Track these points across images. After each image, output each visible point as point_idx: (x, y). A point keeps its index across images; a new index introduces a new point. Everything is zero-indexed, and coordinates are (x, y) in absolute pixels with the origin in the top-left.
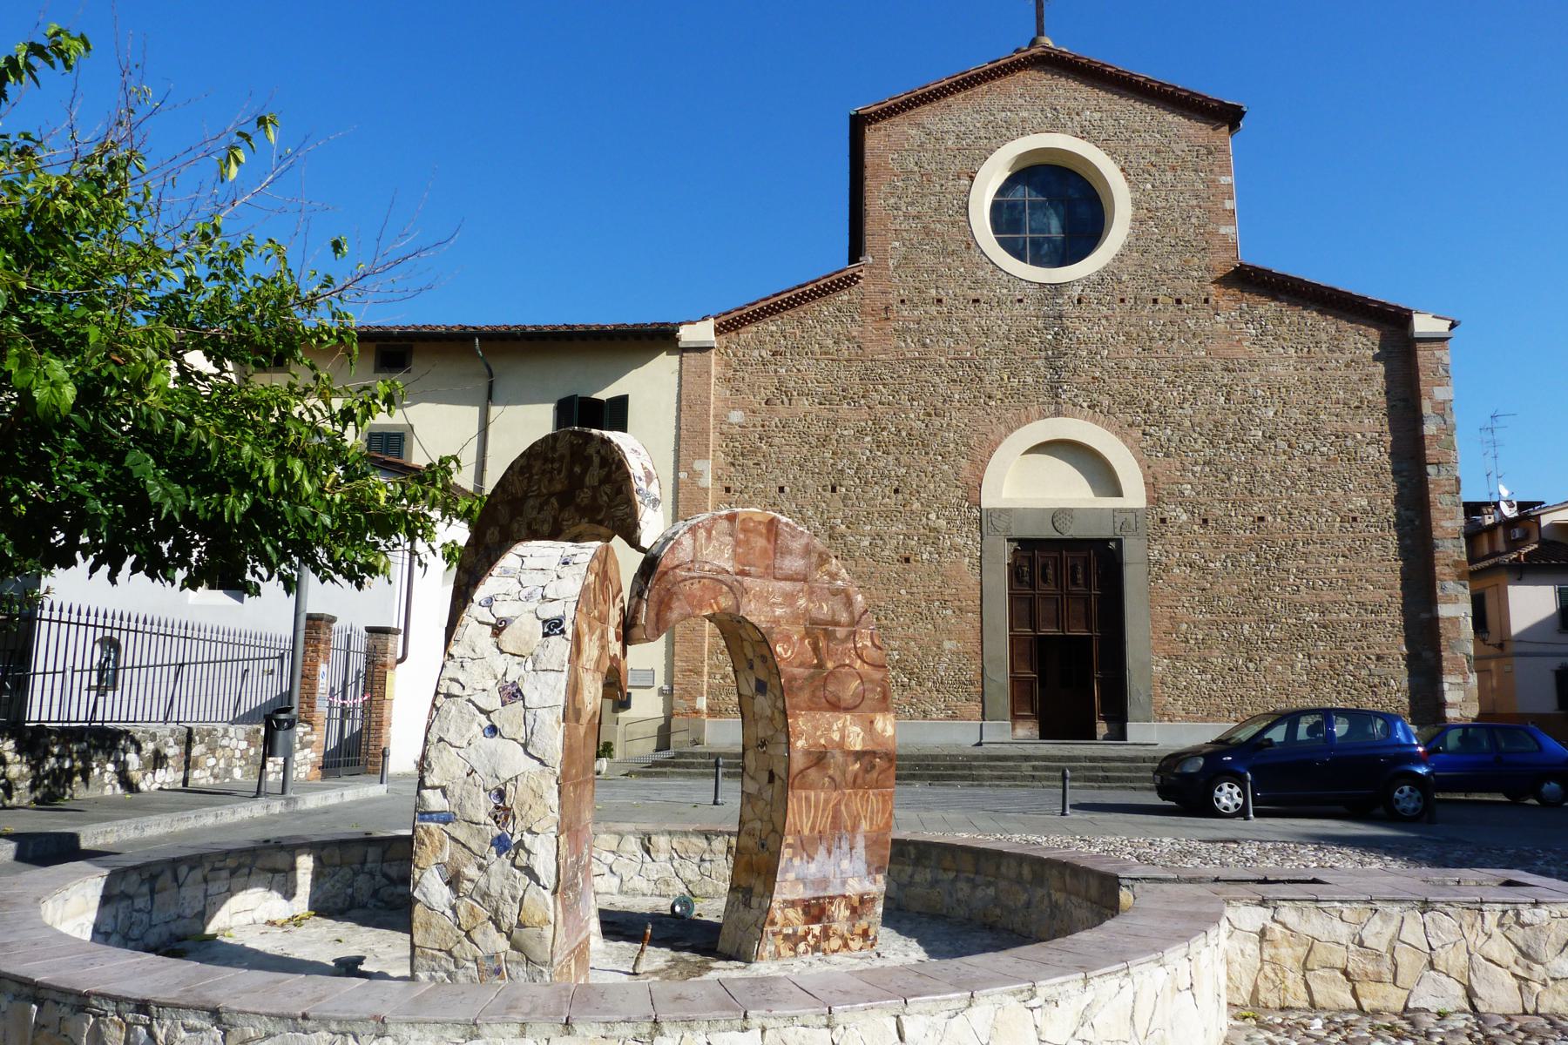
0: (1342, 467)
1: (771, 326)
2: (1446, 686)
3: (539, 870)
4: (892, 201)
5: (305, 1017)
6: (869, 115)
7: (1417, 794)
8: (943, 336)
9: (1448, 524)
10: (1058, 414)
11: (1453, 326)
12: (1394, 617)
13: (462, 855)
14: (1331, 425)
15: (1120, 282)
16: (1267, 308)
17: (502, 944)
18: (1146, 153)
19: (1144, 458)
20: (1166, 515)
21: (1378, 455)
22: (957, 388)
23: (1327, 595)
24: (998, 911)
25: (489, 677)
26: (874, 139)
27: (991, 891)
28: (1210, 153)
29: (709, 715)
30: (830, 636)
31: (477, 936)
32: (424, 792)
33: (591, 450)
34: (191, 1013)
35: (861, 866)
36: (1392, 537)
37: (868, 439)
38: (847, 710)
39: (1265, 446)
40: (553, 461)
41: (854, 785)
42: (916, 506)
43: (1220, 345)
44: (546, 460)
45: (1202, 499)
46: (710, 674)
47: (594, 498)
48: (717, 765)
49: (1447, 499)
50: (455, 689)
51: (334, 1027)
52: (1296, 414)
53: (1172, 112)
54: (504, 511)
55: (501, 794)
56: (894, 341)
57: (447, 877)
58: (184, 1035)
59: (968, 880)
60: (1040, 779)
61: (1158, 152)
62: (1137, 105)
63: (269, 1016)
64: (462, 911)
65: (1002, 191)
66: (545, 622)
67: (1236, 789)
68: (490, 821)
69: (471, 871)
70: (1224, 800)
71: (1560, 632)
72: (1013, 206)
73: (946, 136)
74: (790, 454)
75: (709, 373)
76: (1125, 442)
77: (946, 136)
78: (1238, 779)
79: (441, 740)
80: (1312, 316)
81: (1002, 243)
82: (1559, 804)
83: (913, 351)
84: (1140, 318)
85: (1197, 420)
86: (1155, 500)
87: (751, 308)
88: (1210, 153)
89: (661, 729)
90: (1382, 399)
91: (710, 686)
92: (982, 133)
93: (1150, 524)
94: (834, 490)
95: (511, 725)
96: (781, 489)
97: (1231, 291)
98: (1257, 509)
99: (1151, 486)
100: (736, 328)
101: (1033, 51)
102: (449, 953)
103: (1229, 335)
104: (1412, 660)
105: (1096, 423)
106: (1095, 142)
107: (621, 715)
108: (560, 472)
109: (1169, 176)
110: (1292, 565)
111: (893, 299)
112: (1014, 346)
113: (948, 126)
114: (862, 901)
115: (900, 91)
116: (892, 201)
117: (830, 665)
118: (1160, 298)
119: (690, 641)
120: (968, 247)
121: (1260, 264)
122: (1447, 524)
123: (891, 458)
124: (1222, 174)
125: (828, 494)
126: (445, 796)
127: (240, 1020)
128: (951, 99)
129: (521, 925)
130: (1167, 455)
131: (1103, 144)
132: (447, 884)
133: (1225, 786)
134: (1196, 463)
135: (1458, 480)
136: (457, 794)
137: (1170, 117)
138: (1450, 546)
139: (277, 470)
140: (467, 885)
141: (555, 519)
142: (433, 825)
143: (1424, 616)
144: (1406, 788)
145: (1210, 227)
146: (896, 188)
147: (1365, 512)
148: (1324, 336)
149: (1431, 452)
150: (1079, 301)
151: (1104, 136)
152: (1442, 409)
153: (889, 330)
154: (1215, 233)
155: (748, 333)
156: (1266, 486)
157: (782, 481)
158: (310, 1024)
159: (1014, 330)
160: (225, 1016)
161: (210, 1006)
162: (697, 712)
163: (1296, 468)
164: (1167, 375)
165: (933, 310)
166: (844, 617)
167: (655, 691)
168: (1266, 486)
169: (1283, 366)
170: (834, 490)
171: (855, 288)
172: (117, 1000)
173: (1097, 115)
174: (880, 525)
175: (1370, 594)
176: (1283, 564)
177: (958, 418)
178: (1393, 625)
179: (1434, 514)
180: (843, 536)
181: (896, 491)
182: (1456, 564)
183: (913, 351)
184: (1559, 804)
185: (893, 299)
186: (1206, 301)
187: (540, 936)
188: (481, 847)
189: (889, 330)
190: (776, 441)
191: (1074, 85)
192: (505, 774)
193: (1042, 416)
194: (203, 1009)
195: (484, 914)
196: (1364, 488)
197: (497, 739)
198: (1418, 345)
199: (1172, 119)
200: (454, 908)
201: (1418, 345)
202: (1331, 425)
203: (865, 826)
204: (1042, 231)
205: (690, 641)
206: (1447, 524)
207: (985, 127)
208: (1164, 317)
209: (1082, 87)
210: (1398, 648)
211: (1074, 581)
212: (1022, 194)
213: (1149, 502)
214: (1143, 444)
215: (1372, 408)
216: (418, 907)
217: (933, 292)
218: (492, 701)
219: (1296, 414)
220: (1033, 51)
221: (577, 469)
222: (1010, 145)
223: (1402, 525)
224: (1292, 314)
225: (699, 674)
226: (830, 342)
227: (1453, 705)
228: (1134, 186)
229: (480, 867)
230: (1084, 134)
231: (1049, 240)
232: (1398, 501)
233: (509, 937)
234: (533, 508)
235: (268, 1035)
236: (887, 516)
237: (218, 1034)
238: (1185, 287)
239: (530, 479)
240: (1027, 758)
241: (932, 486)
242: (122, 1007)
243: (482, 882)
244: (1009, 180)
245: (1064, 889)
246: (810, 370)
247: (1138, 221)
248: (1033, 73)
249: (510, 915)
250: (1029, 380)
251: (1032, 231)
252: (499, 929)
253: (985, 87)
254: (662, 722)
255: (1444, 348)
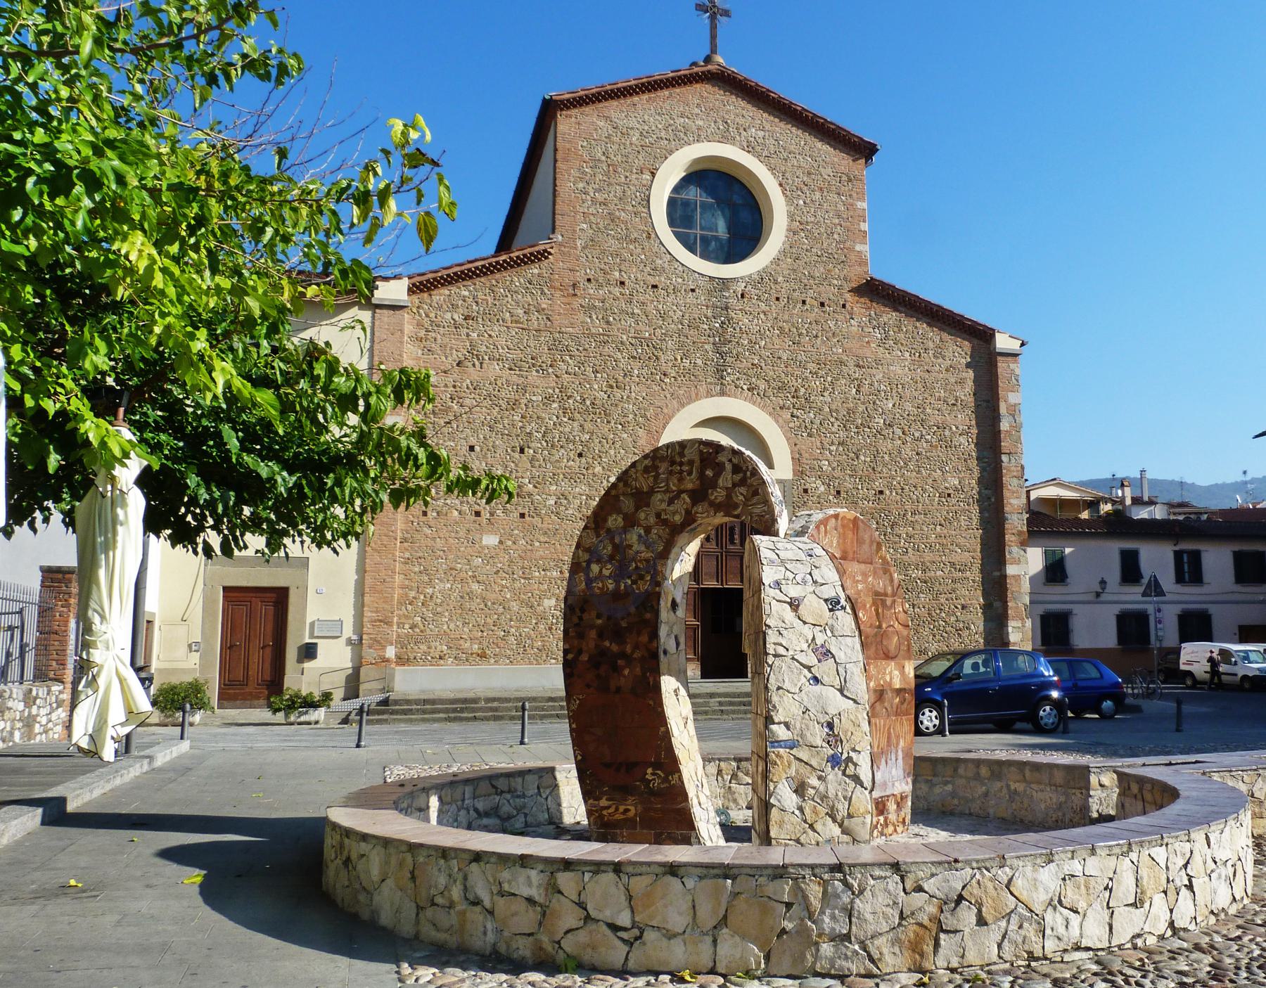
0: (941, 453)
1: (463, 291)
2: (1010, 629)
3: (863, 777)
4: (581, 185)
5: (956, 861)
6: (562, 101)
7: (1055, 712)
8: (623, 316)
9: (1014, 504)
10: (722, 393)
11: (1022, 345)
12: (975, 574)
13: (804, 770)
14: (934, 418)
15: (776, 282)
16: (890, 317)
17: (836, 831)
18: (799, 172)
19: (792, 435)
20: (808, 486)
21: (967, 444)
22: (636, 365)
23: (928, 556)
24: (956, 801)
25: (803, 641)
26: (566, 124)
27: (949, 788)
28: (850, 180)
29: (397, 664)
30: (883, 602)
31: (818, 827)
32: (773, 727)
33: (722, 458)
34: (876, 868)
35: (901, 772)
36: (975, 510)
37: (555, 405)
38: (892, 658)
39: (885, 432)
40: (681, 464)
41: (897, 714)
42: (598, 469)
43: (851, 344)
44: (673, 463)
45: (837, 473)
46: (398, 624)
47: (729, 496)
48: (523, 709)
49: (1015, 481)
50: (781, 651)
51: (975, 865)
52: (908, 406)
53: (821, 140)
54: (627, 504)
55: (830, 725)
56: (581, 316)
57: (794, 787)
58: (872, 882)
59: (927, 781)
60: (728, 713)
61: (809, 173)
62: (794, 130)
63: (932, 863)
64: (807, 811)
65: (677, 189)
66: (826, 600)
67: (935, 713)
68: (825, 745)
69: (814, 781)
70: (926, 722)
71: (1121, 585)
72: (686, 204)
73: (631, 132)
74: (480, 415)
75: (402, 331)
76: (777, 422)
77: (631, 132)
78: (938, 706)
79: (779, 688)
80: (923, 327)
81: (677, 235)
82: (1111, 717)
83: (598, 327)
84: (791, 315)
85: (834, 407)
86: (799, 473)
87: (445, 272)
88: (850, 180)
89: (348, 677)
90: (971, 399)
91: (398, 636)
92: (663, 134)
93: (795, 493)
94: (522, 451)
95: (828, 676)
96: (472, 448)
97: (862, 300)
98: (878, 484)
99: (797, 460)
100: (429, 289)
101: (710, 67)
102: (798, 841)
103: (861, 337)
104: (987, 608)
105: (754, 403)
106: (758, 157)
107: (307, 665)
108: (690, 473)
109: (818, 195)
110: (902, 531)
111: (580, 277)
112: (686, 331)
113: (633, 123)
114: (902, 798)
115: (591, 84)
116: (581, 185)
117: (884, 626)
118: (808, 300)
119: (380, 592)
120: (649, 237)
121: (886, 280)
122: (1014, 502)
123: (576, 424)
124: (859, 199)
125: (517, 455)
126: (788, 729)
127: (913, 868)
128: (636, 99)
129: (850, 816)
130: (810, 435)
131: (765, 159)
132: (796, 791)
133: (926, 711)
134: (832, 443)
135: (1022, 467)
136: (798, 726)
137: (819, 145)
138: (1016, 521)
139: (427, 458)
140: (811, 792)
141: (688, 512)
142: (781, 750)
143: (997, 574)
144: (1048, 708)
145: (848, 244)
146: (584, 173)
147: (956, 490)
148: (931, 345)
149: (1004, 444)
150: (742, 296)
151: (765, 153)
152: (1014, 411)
153: (576, 305)
154: (851, 249)
155: (440, 295)
156: (885, 465)
157: (473, 441)
158: (959, 865)
159: (687, 316)
160: (903, 867)
161: (891, 860)
162: (388, 660)
163: (908, 451)
164: (811, 366)
165: (617, 291)
166: (889, 590)
167: (342, 640)
168: (885, 465)
169: (900, 367)
170: (522, 451)
171: (545, 263)
172: (812, 867)
173: (761, 134)
174: (565, 485)
175: (961, 557)
176: (897, 530)
177: (637, 392)
178: (974, 581)
179: (1006, 493)
180: (530, 495)
181: (580, 455)
182: (1020, 533)
183: (598, 327)
184: (1111, 717)
185: (580, 277)
186: (844, 306)
187: (864, 823)
188: (820, 764)
189: (576, 305)
190: (467, 402)
191: (743, 103)
192: (832, 711)
193: (709, 394)
194: (886, 864)
195: (822, 810)
196: (956, 470)
197: (819, 686)
198: (999, 358)
199: (823, 149)
200: (801, 809)
201: (999, 358)
202: (934, 418)
203: (902, 743)
204: (710, 230)
205: (380, 592)
206: (1014, 502)
207: (666, 129)
208: (811, 317)
209: (749, 106)
210: (977, 599)
211: (732, 542)
212: (694, 194)
213: (794, 475)
214: (792, 425)
215: (964, 406)
216: (774, 811)
217: (617, 274)
218: (811, 659)
219: (908, 406)
220: (710, 67)
221: (709, 473)
222: (686, 149)
223: (982, 501)
224: (909, 324)
225: (389, 624)
226: (520, 312)
227: (1015, 644)
228: (789, 200)
229: (820, 778)
230: (749, 148)
231: (716, 238)
232: (980, 482)
233: (841, 826)
234: (662, 501)
235: (933, 875)
236: (571, 477)
237: (897, 878)
238: (828, 293)
239: (656, 477)
240: (712, 695)
241: (612, 452)
242: (817, 871)
243: (822, 789)
244: (683, 179)
245: (1024, 780)
246: (501, 337)
247: (792, 231)
248: (708, 87)
249: (842, 808)
250: (699, 362)
251: (702, 229)
252: (834, 821)
253: (666, 92)
254: (350, 671)
255: (1016, 362)
